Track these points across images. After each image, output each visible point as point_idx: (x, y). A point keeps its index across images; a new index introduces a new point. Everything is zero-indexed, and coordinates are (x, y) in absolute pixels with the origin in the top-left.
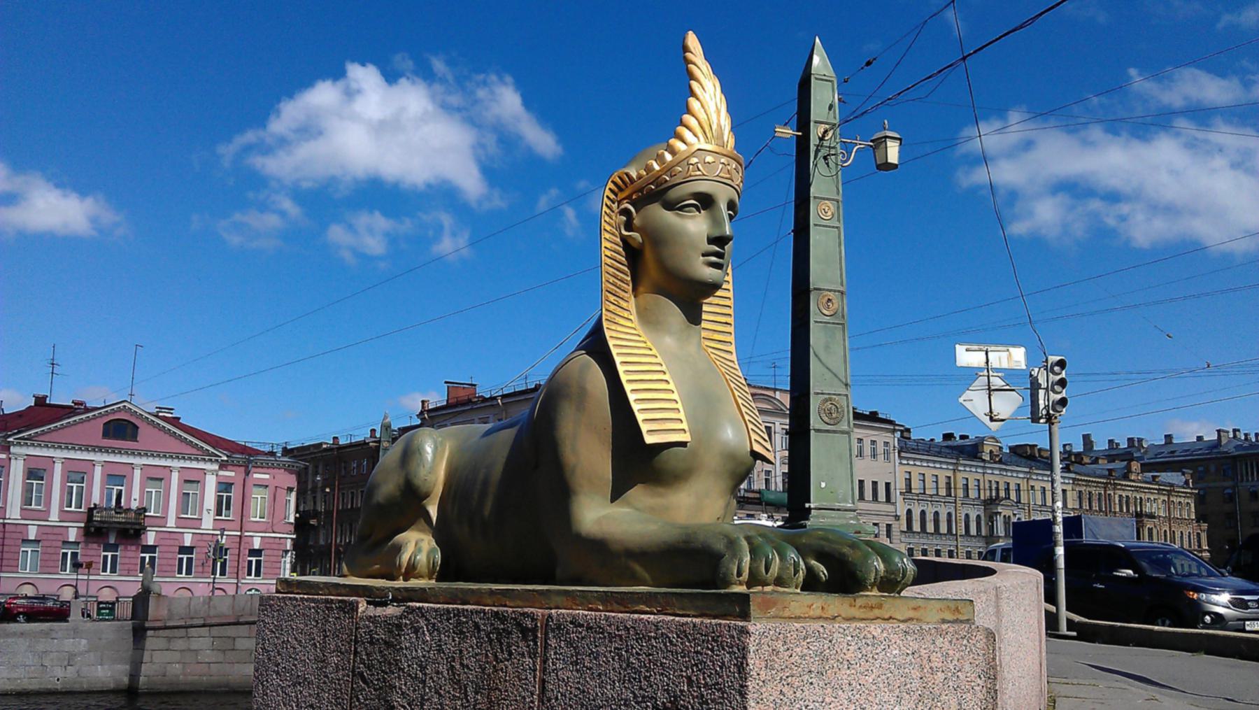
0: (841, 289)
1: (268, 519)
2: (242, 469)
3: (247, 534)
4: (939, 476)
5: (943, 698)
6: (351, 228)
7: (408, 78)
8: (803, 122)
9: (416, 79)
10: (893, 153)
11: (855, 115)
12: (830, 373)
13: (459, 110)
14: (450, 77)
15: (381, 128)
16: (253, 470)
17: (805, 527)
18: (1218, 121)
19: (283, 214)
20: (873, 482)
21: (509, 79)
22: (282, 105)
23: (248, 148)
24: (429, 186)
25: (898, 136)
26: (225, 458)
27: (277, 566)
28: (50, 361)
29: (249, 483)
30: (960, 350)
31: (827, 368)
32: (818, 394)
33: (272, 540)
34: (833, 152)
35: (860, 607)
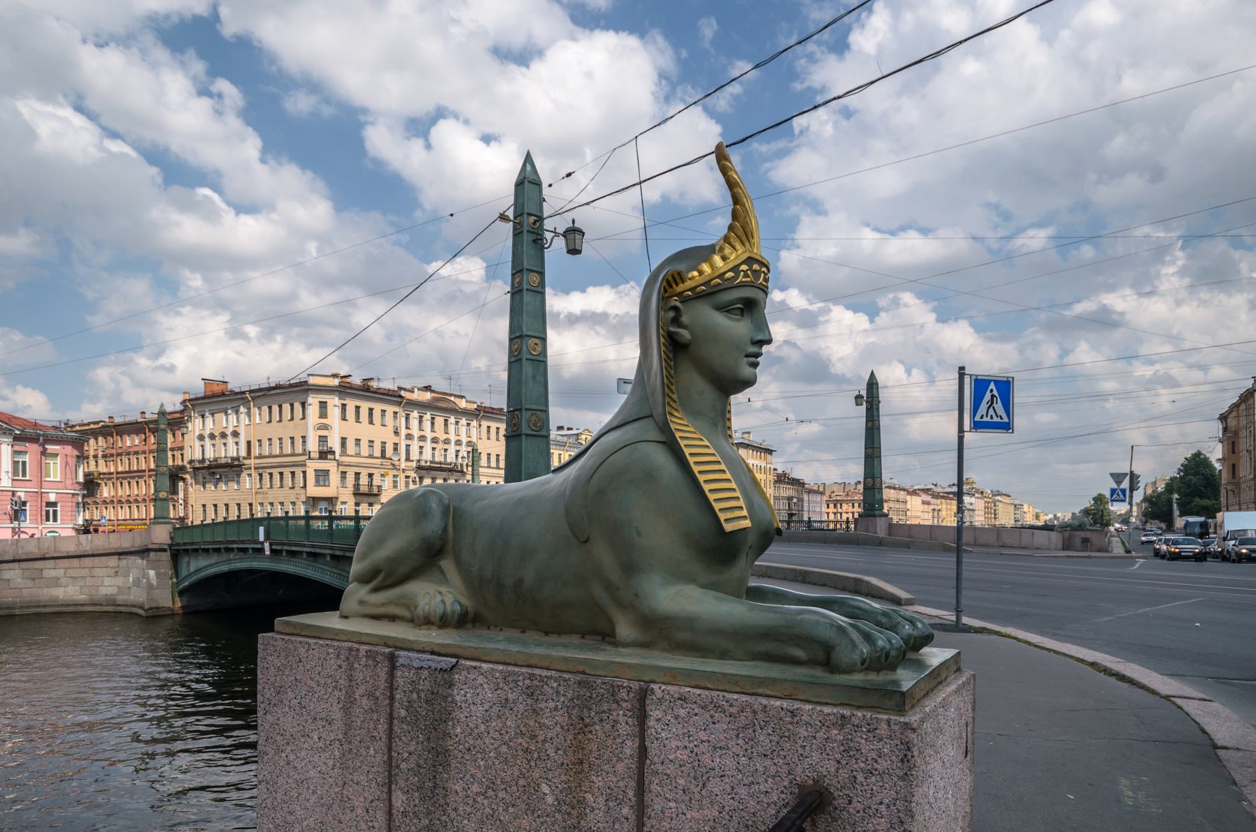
4: (443, 432)
17: (1220, 470)
18: (685, 334)
20: (342, 438)
30: (750, 525)
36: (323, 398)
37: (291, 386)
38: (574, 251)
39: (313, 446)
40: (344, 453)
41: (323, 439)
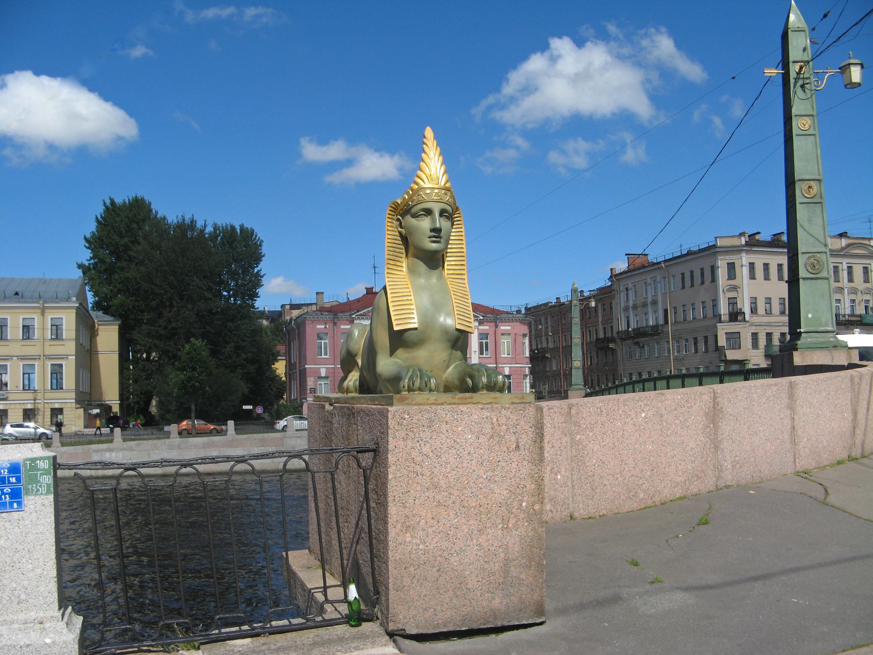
0: (818, 177)
1: (512, 355)
2: (493, 324)
3: (499, 365)
5: (506, 437)
6: (563, 152)
7: (592, 42)
8: (785, 64)
9: (597, 41)
10: (856, 74)
11: (816, 55)
12: (813, 239)
13: (629, 57)
14: (621, 36)
15: (577, 79)
16: (500, 324)
19: (517, 148)
21: (663, 29)
22: (509, 75)
23: (490, 108)
24: (614, 114)
25: (860, 62)
26: (482, 318)
27: (520, 385)
28: (373, 266)
29: (499, 333)
31: (811, 235)
32: (805, 253)
33: (516, 369)
34: (808, 81)
35: (459, 399)
36: (731, 258)
37: (701, 251)
39: (724, 309)
40: (754, 311)
41: (732, 302)
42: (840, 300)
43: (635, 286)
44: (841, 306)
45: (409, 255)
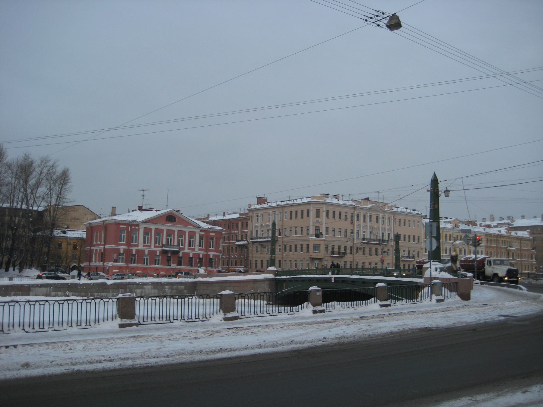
28: (142, 195)
38: (447, 196)
41: (317, 229)
42: (365, 231)
43: (262, 215)
44: (366, 234)
45: (68, 178)
